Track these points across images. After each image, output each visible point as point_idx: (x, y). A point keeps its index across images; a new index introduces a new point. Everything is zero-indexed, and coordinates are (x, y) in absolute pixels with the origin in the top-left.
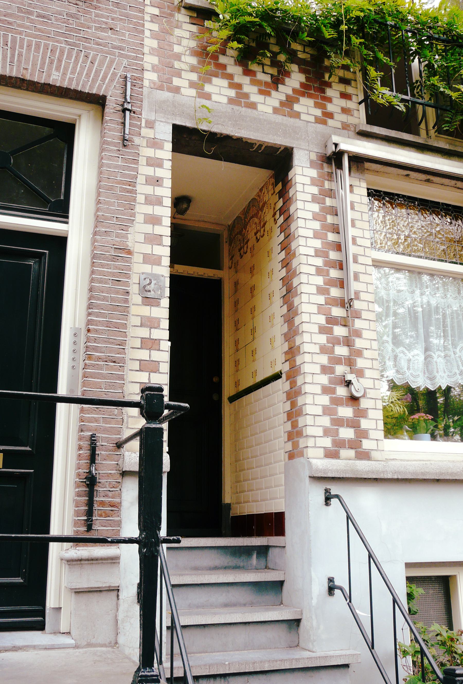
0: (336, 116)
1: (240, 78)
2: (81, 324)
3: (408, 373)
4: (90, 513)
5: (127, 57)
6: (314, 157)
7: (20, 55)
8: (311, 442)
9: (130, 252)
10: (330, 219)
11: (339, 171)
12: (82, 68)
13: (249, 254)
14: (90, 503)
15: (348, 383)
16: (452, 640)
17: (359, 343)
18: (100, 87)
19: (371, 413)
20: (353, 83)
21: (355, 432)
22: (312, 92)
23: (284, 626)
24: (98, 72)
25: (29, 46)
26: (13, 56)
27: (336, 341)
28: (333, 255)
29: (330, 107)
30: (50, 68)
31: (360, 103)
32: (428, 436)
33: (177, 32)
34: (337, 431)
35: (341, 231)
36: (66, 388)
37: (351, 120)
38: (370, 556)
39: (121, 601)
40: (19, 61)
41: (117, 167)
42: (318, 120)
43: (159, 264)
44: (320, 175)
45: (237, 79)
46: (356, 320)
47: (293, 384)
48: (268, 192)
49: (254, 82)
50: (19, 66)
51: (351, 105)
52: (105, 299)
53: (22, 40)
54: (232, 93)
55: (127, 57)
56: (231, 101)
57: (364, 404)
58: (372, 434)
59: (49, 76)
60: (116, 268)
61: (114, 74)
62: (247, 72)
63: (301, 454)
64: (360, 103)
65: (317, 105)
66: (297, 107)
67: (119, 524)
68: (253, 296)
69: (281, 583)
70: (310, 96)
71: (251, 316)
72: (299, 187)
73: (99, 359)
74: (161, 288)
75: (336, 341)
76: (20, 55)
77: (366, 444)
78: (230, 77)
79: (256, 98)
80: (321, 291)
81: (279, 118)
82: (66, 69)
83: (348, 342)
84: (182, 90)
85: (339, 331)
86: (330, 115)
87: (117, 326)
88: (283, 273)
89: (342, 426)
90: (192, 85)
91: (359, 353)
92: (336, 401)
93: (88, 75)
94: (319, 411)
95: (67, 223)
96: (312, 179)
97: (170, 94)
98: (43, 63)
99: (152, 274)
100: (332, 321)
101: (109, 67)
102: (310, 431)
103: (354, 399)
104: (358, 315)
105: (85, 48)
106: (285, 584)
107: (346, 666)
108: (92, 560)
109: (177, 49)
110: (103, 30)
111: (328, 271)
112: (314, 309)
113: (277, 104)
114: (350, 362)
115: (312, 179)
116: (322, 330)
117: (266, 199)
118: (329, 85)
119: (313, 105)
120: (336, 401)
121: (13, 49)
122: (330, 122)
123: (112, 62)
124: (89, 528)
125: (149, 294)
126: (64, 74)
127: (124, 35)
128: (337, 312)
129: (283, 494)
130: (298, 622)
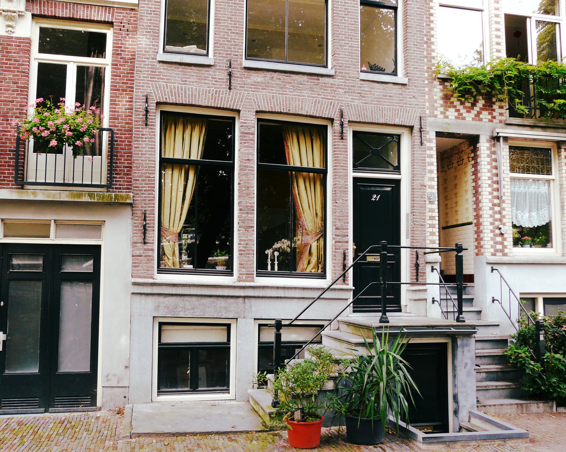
0: (497, 117)
1: (460, 107)
2: (409, 211)
3: (522, 222)
4: (417, 275)
5: (420, 108)
6: (488, 138)
7: (385, 114)
8: (486, 250)
9: (425, 186)
10: (494, 164)
11: (498, 143)
12: (406, 115)
13: (453, 169)
14: (417, 272)
15: (500, 229)
16: (536, 315)
17: (504, 213)
18: (412, 123)
19: (508, 239)
20: (504, 101)
21: (502, 247)
22: (487, 108)
23: (476, 313)
24: (411, 116)
25: (387, 110)
26: (382, 114)
27: (495, 213)
28: (495, 179)
29: (495, 114)
30: (395, 118)
31: (507, 109)
32: (529, 246)
33: (435, 90)
34: (495, 246)
35: (498, 168)
36: (320, 206)
37: (503, 118)
38: (510, 289)
39: (427, 303)
40: (385, 116)
41: (419, 154)
42: (491, 121)
43: (433, 188)
44: (491, 146)
45: (458, 108)
46: (503, 204)
47: (478, 228)
48: (465, 146)
49: (465, 108)
50: (385, 118)
51: (503, 111)
52: (418, 204)
53: (385, 107)
54: (456, 114)
55: (420, 108)
56: (456, 118)
57: (505, 236)
58: (508, 247)
59: (395, 121)
60: (421, 192)
61: (416, 116)
62: (462, 103)
63: (482, 254)
64: (507, 109)
65: (489, 114)
66: (481, 116)
67: (426, 279)
68: (456, 188)
69: (473, 299)
70: (486, 110)
71: (455, 196)
72: (482, 152)
73: (417, 225)
74: (435, 198)
75: (495, 213)
76: (385, 114)
77: (506, 251)
78: (455, 107)
79: (465, 115)
80: (491, 193)
81: (474, 122)
82: (400, 117)
83: (500, 213)
84: (438, 116)
85: (497, 209)
86: (494, 117)
87: (423, 213)
88: (474, 184)
89: (497, 244)
90: (442, 113)
91: (504, 217)
92: (496, 235)
93: (407, 118)
94: (489, 239)
95: (400, 175)
96: (487, 147)
97: (434, 118)
98: (392, 116)
99: (431, 192)
100: (494, 205)
101: (414, 113)
102: (486, 246)
103: (502, 234)
104: (504, 202)
105: (406, 107)
106: (474, 300)
107: (498, 325)
108: (419, 290)
109: (435, 98)
110: (411, 98)
111: (493, 185)
112: (488, 201)
113: (473, 116)
114: (501, 220)
115: (487, 147)
116: (491, 209)
117: (464, 149)
118: (494, 103)
119: (487, 114)
120: (496, 235)
121: (382, 112)
122: (494, 120)
123: (415, 111)
124: (417, 280)
125: (431, 200)
126: (400, 119)
127: (418, 99)
128: (496, 201)
129: (473, 268)
130: (480, 312)
